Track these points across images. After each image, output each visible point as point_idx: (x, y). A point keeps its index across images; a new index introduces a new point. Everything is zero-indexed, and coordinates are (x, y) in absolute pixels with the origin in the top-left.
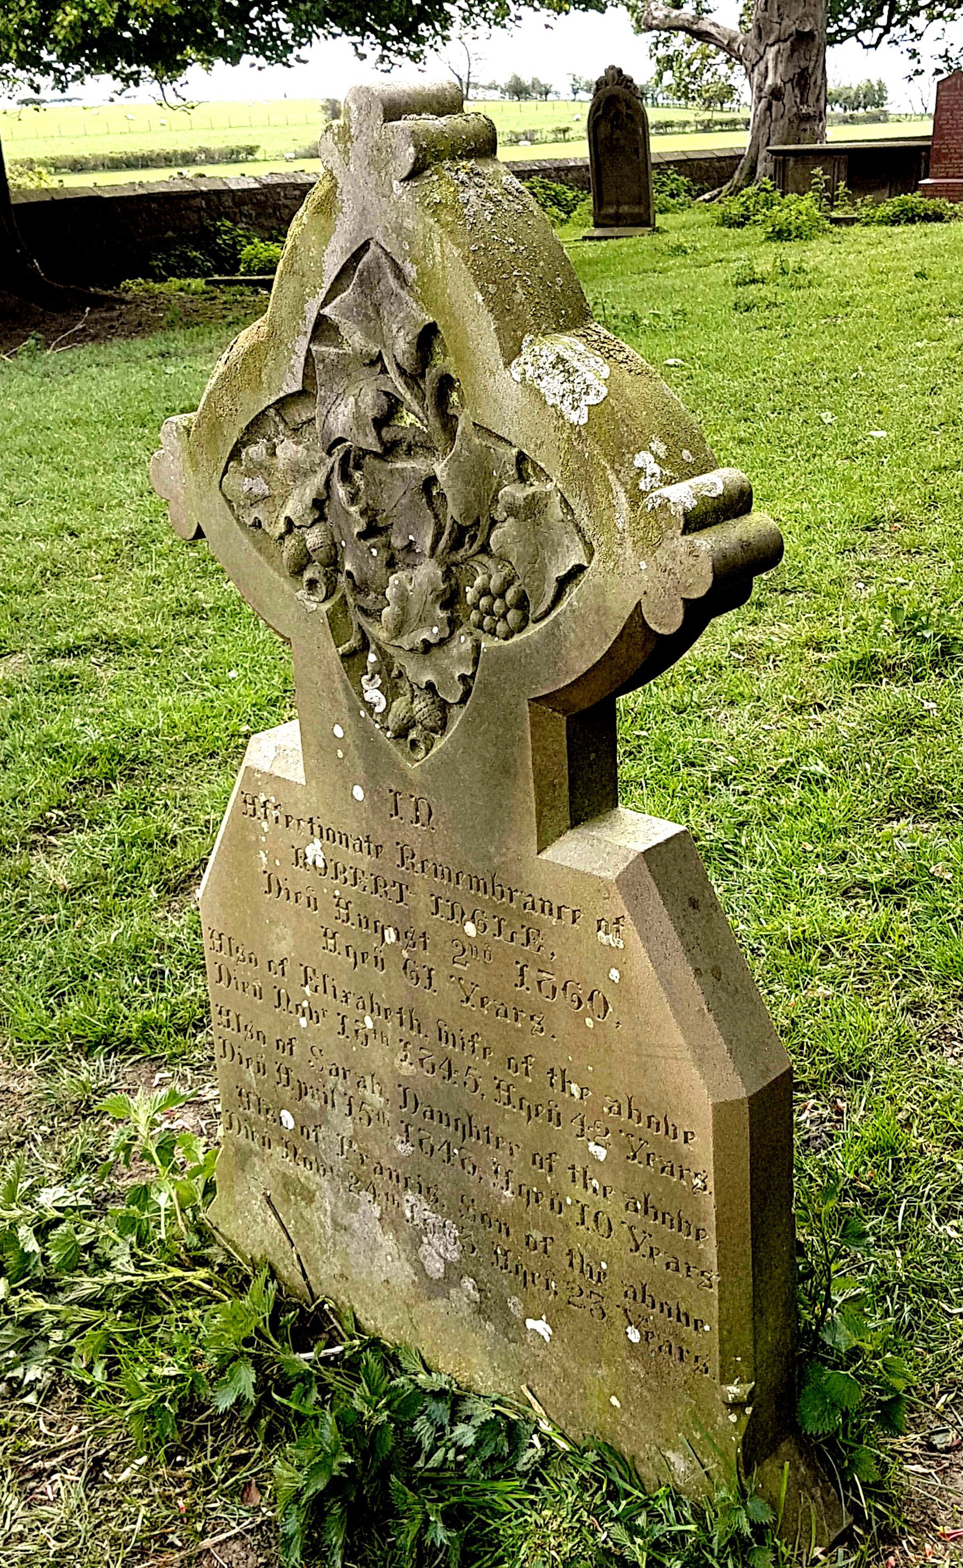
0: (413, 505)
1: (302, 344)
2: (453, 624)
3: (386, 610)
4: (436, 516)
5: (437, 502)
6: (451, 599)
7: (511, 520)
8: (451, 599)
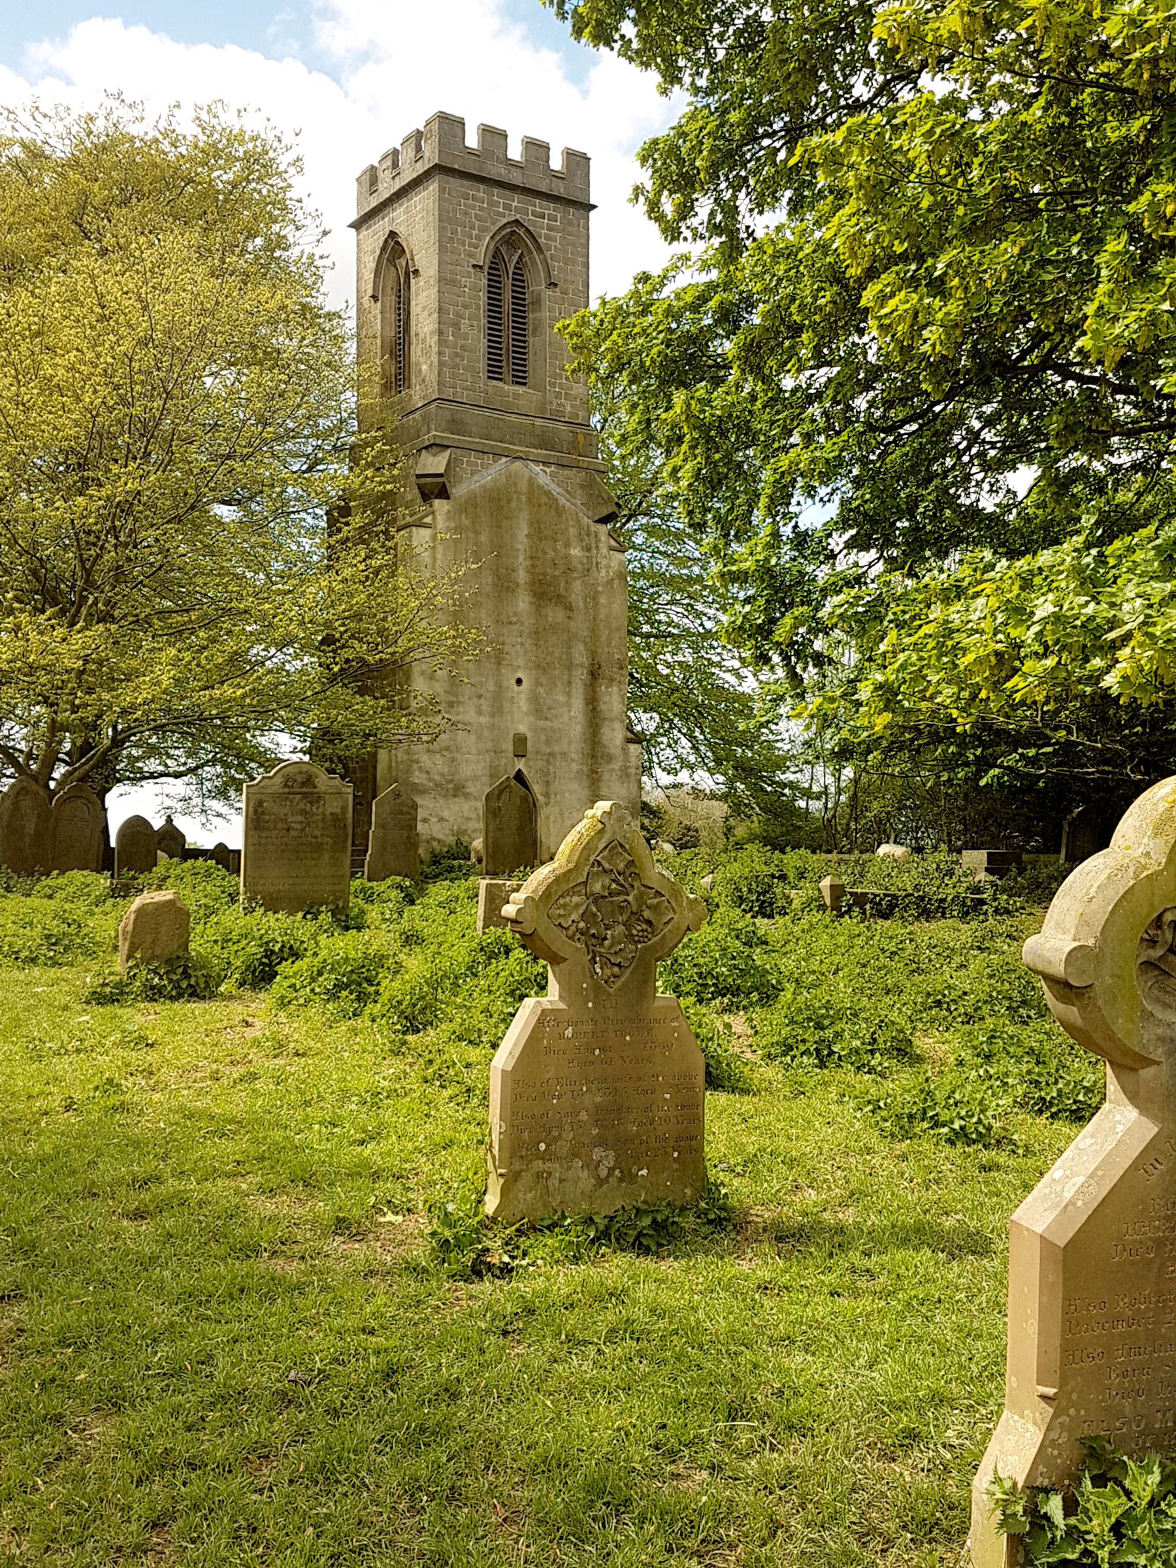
1: (587, 868)
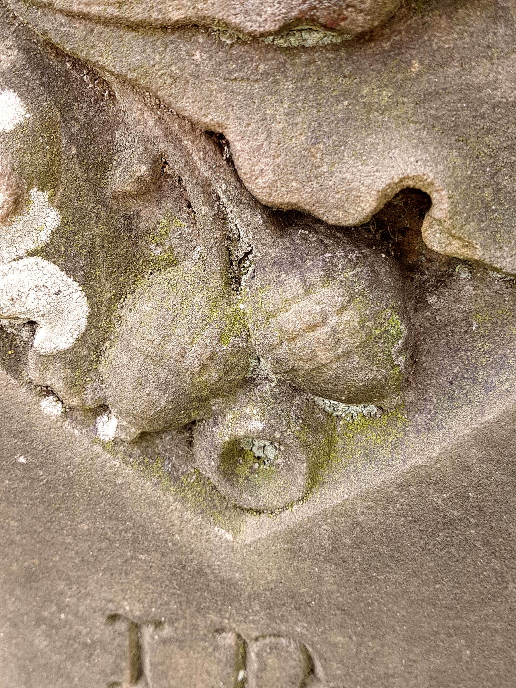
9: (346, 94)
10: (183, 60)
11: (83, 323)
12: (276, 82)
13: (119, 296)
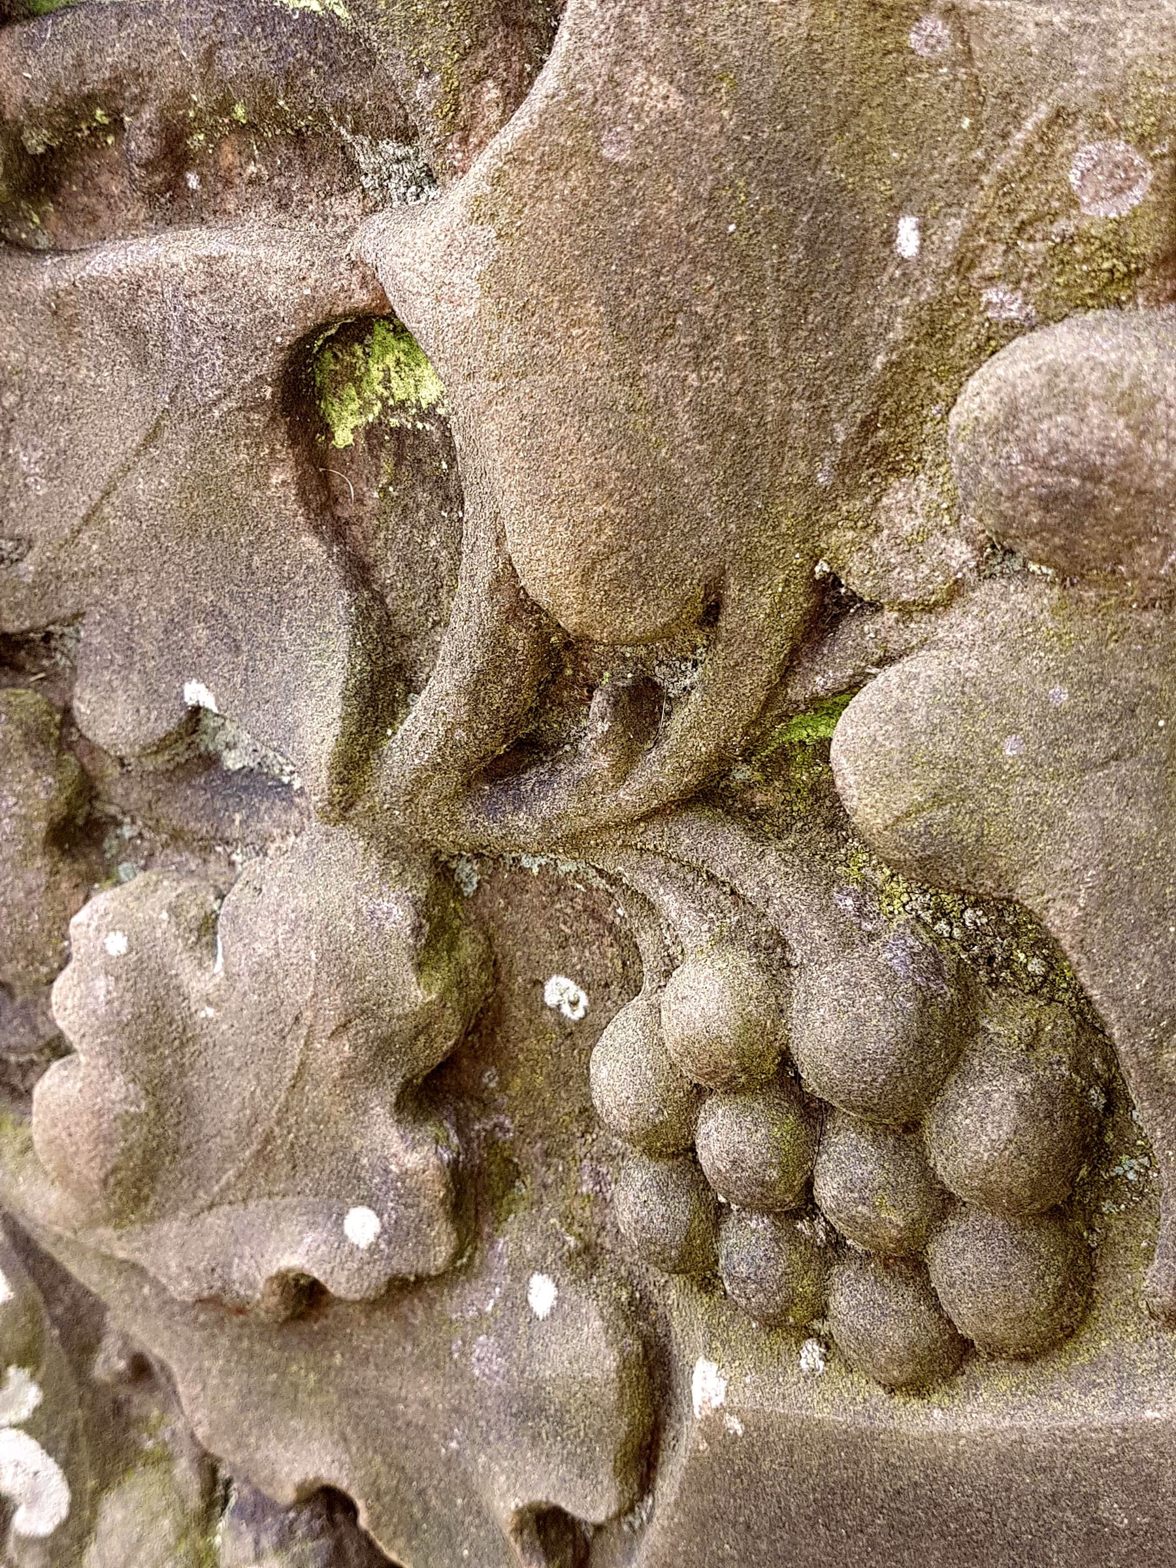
0: (209, 512)
2: (474, 1195)
3: (54, 1087)
4: (359, 572)
5: (367, 493)
6: (466, 1071)
7: (1022, 599)
8: (466, 1071)
9: (275, 1367)
10: (132, 1290)
11: (64, 1512)
12: (214, 1336)
13: (104, 1485)
